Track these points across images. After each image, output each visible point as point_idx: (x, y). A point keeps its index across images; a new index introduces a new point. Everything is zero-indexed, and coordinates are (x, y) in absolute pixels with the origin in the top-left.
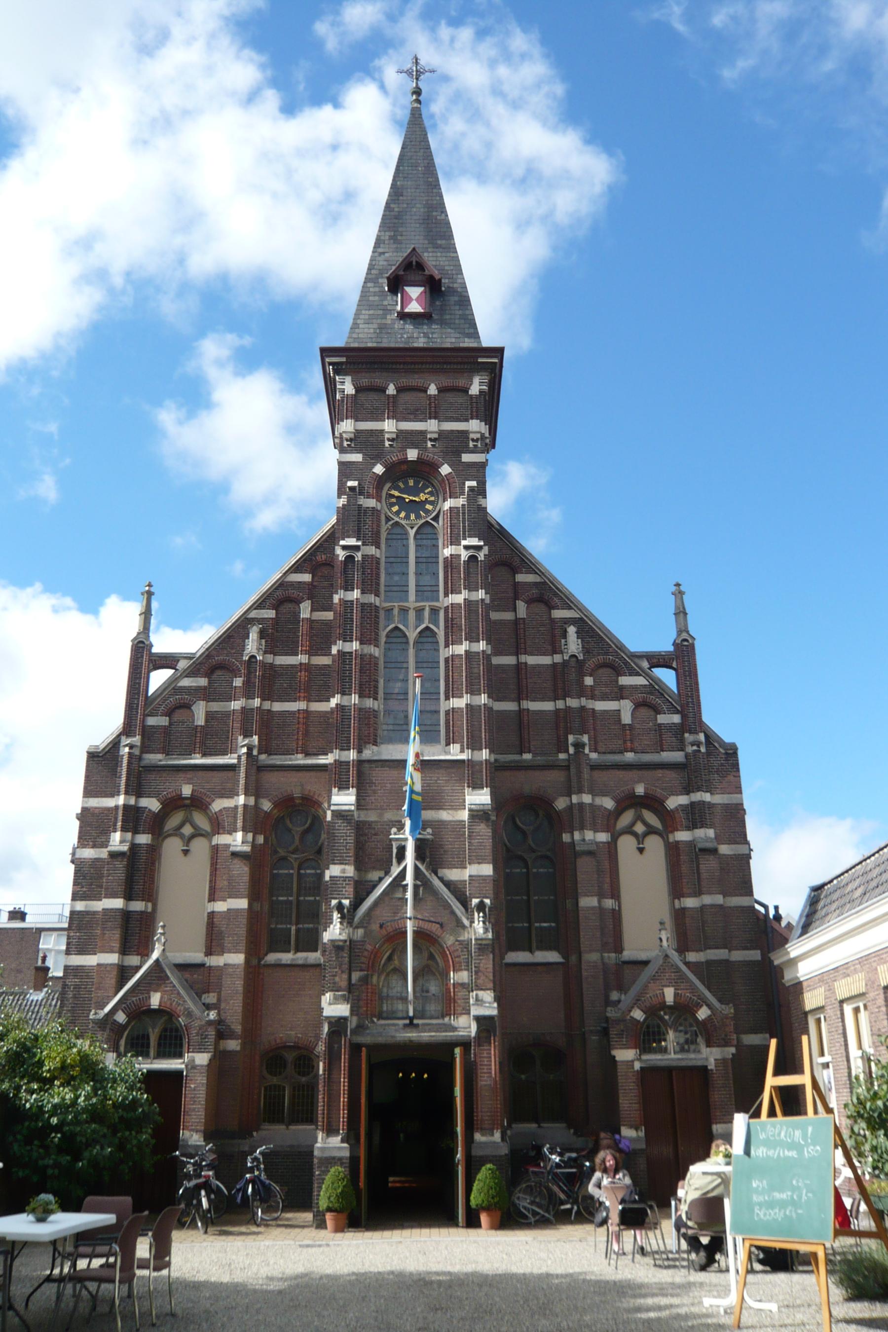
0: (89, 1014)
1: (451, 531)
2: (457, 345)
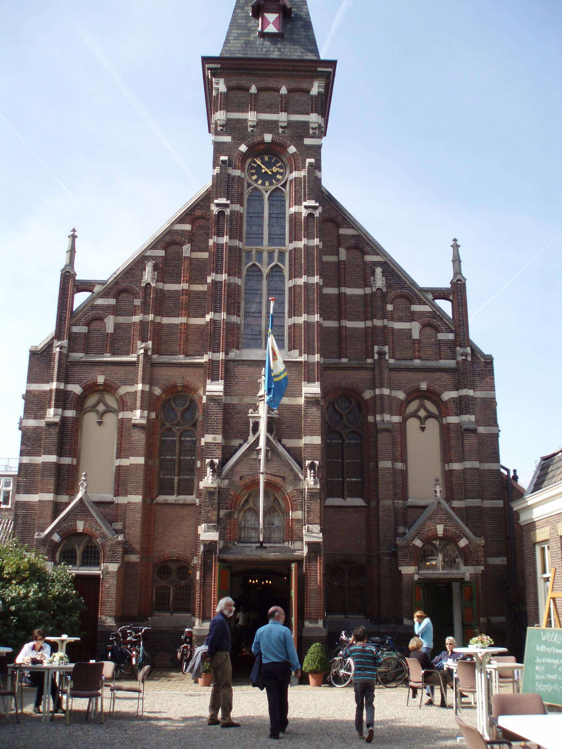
1: (295, 195)
2: (302, 58)
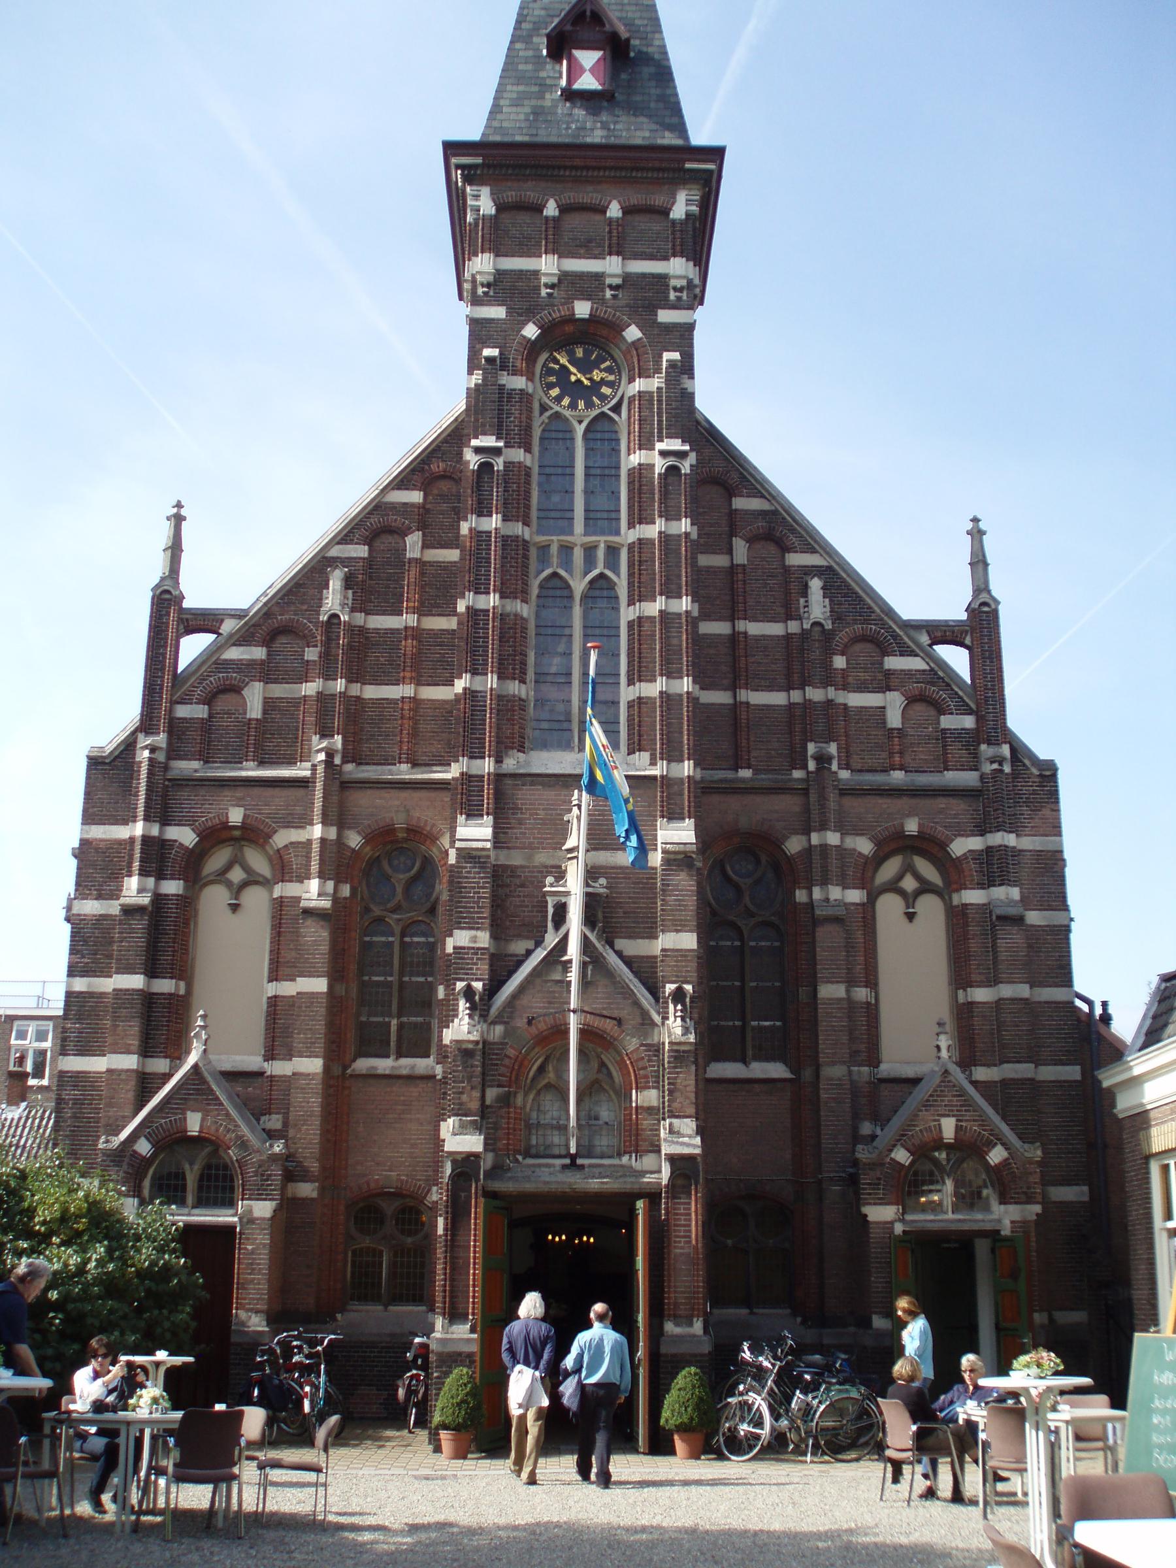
0: (98, 1140)
1: (640, 428)
